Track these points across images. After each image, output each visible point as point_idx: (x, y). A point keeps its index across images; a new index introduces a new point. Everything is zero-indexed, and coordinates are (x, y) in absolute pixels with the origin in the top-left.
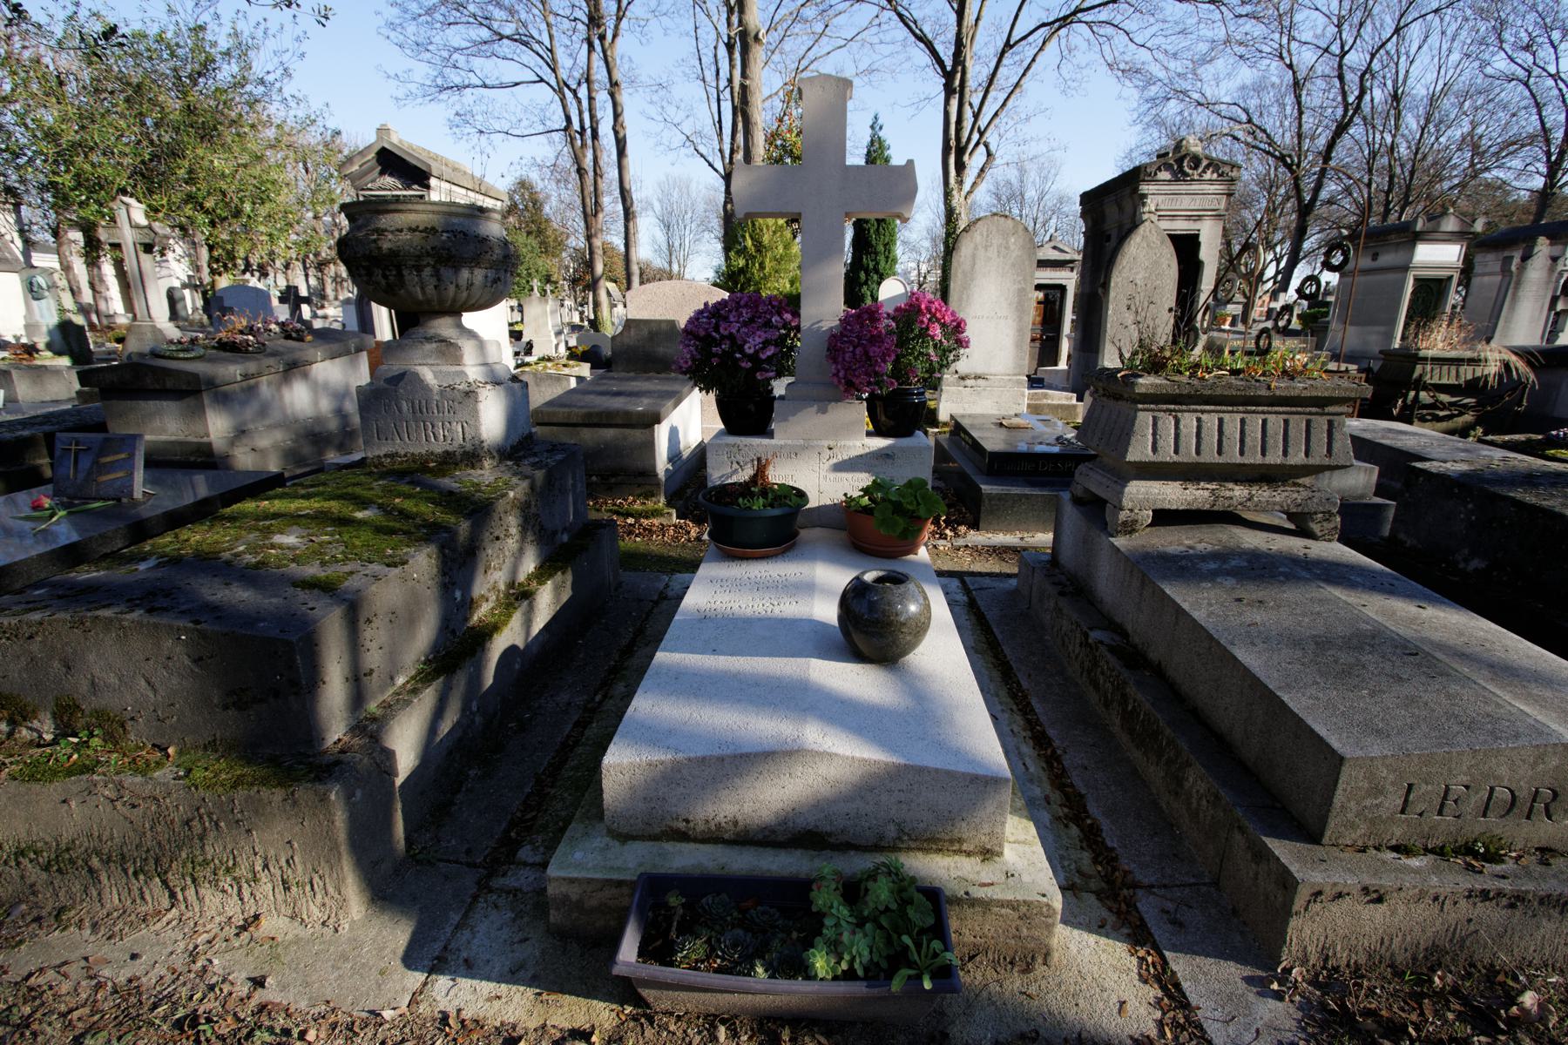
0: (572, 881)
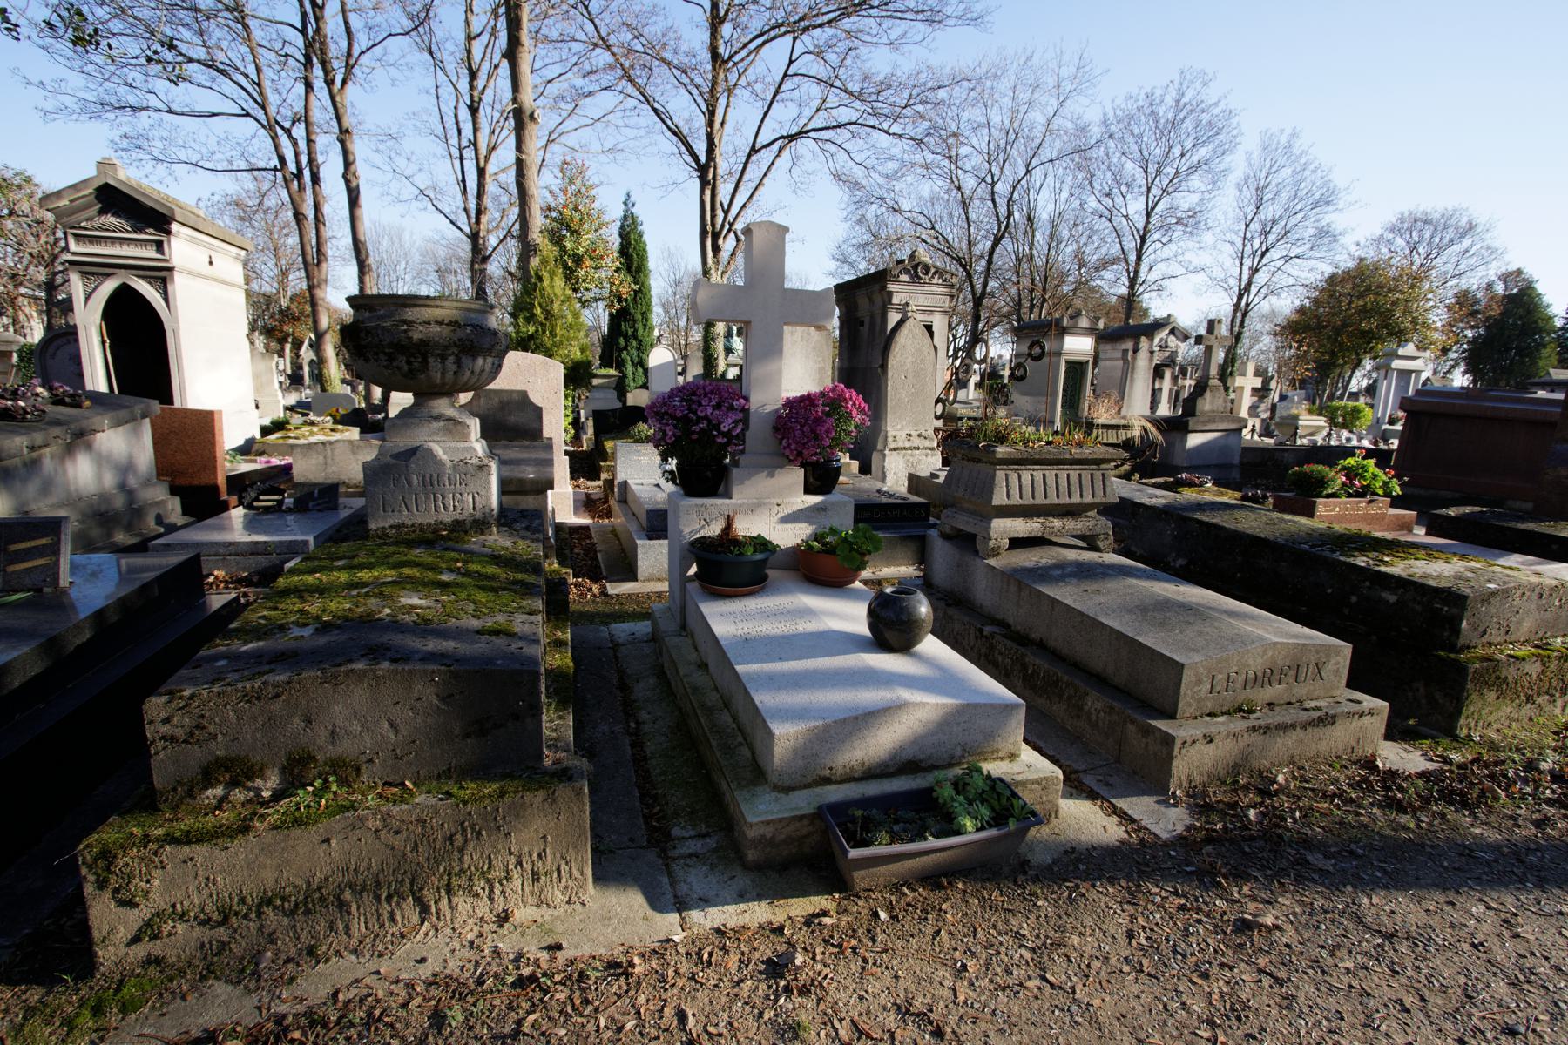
0: (768, 823)
